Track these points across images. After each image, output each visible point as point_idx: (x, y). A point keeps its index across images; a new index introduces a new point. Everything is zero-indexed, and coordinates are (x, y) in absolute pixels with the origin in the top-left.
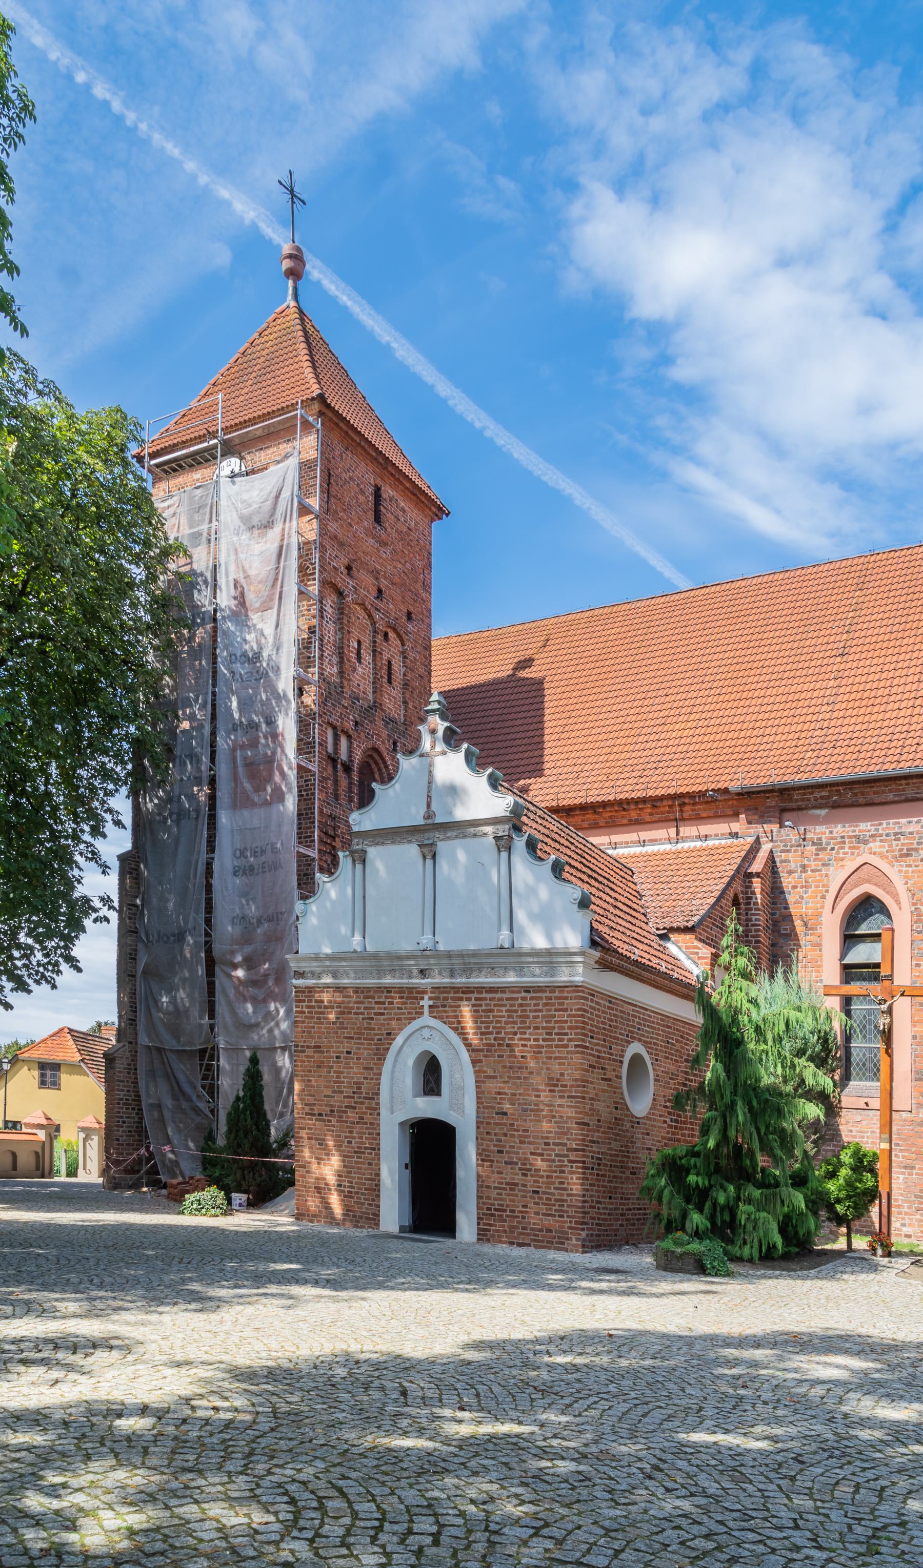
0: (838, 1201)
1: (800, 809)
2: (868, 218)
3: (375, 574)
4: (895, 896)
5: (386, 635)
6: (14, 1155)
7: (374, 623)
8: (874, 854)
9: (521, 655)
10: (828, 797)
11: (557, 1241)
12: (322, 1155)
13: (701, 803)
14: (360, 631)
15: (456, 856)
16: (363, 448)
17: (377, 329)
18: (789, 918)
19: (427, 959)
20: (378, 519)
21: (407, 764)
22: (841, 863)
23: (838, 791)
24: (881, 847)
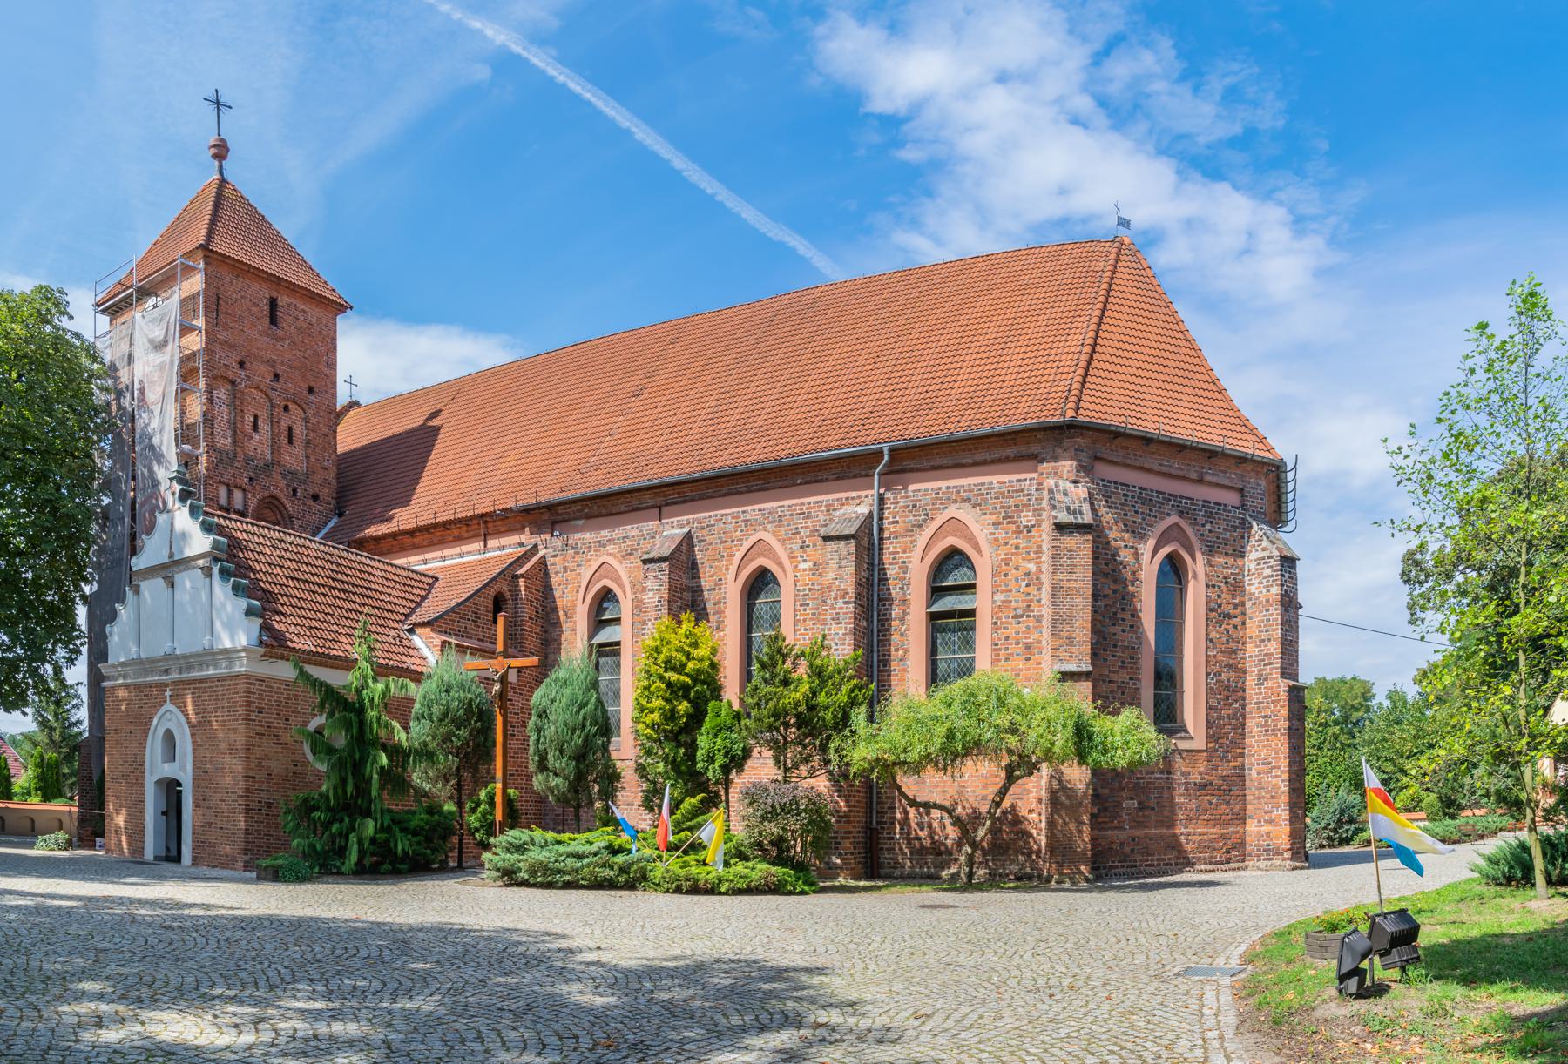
0: (477, 830)
2: (1077, 57)
4: (621, 586)
5: (286, 408)
6: (32, 821)
8: (610, 555)
9: (432, 409)
11: (228, 864)
12: (118, 811)
14: (256, 404)
15: (188, 581)
17: (618, 118)
18: (555, 609)
19: (169, 657)
20: (273, 320)
21: (161, 519)
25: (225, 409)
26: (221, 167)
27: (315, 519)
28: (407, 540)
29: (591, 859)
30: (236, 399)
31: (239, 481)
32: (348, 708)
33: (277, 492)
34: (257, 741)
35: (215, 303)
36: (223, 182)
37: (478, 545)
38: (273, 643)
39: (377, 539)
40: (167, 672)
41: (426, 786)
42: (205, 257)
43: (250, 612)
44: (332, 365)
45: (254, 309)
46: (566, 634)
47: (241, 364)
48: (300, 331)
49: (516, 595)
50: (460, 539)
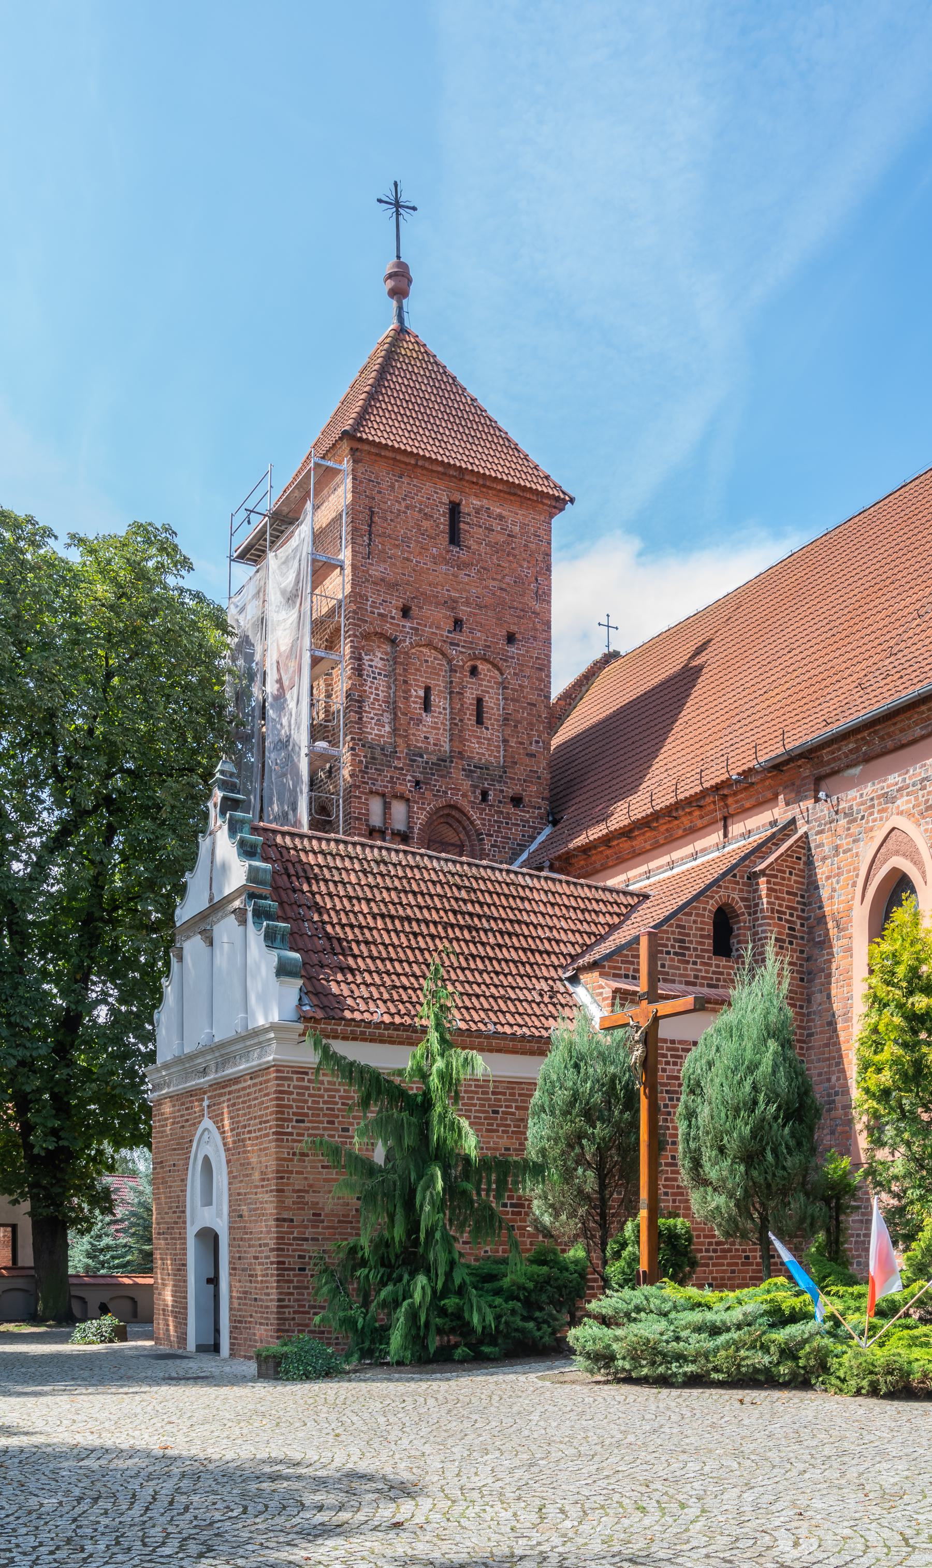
1: (834, 773)
3: (450, 605)
5: (474, 671)
7: (450, 661)
9: (699, 641)
10: (857, 749)
13: (741, 791)
14: (428, 670)
16: (423, 468)
18: (822, 920)
20: (454, 537)
22: (871, 834)
23: (863, 739)
24: (908, 802)
25: (381, 682)
26: (400, 308)
27: (516, 833)
28: (624, 845)
29: (735, 1335)
30: (399, 666)
31: (400, 788)
32: (407, 1108)
33: (458, 799)
34: (295, 1165)
35: (366, 521)
36: (402, 331)
37: (716, 837)
38: (322, 1013)
39: (586, 850)
40: (204, 1072)
41: (547, 1219)
42: (353, 451)
43: (283, 970)
44: (544, 596)
45: (426, 524)
46: (839, 962)
47: (406, 612)
48: (496, 548)
49: (753, 906)
50: (693, 832)
